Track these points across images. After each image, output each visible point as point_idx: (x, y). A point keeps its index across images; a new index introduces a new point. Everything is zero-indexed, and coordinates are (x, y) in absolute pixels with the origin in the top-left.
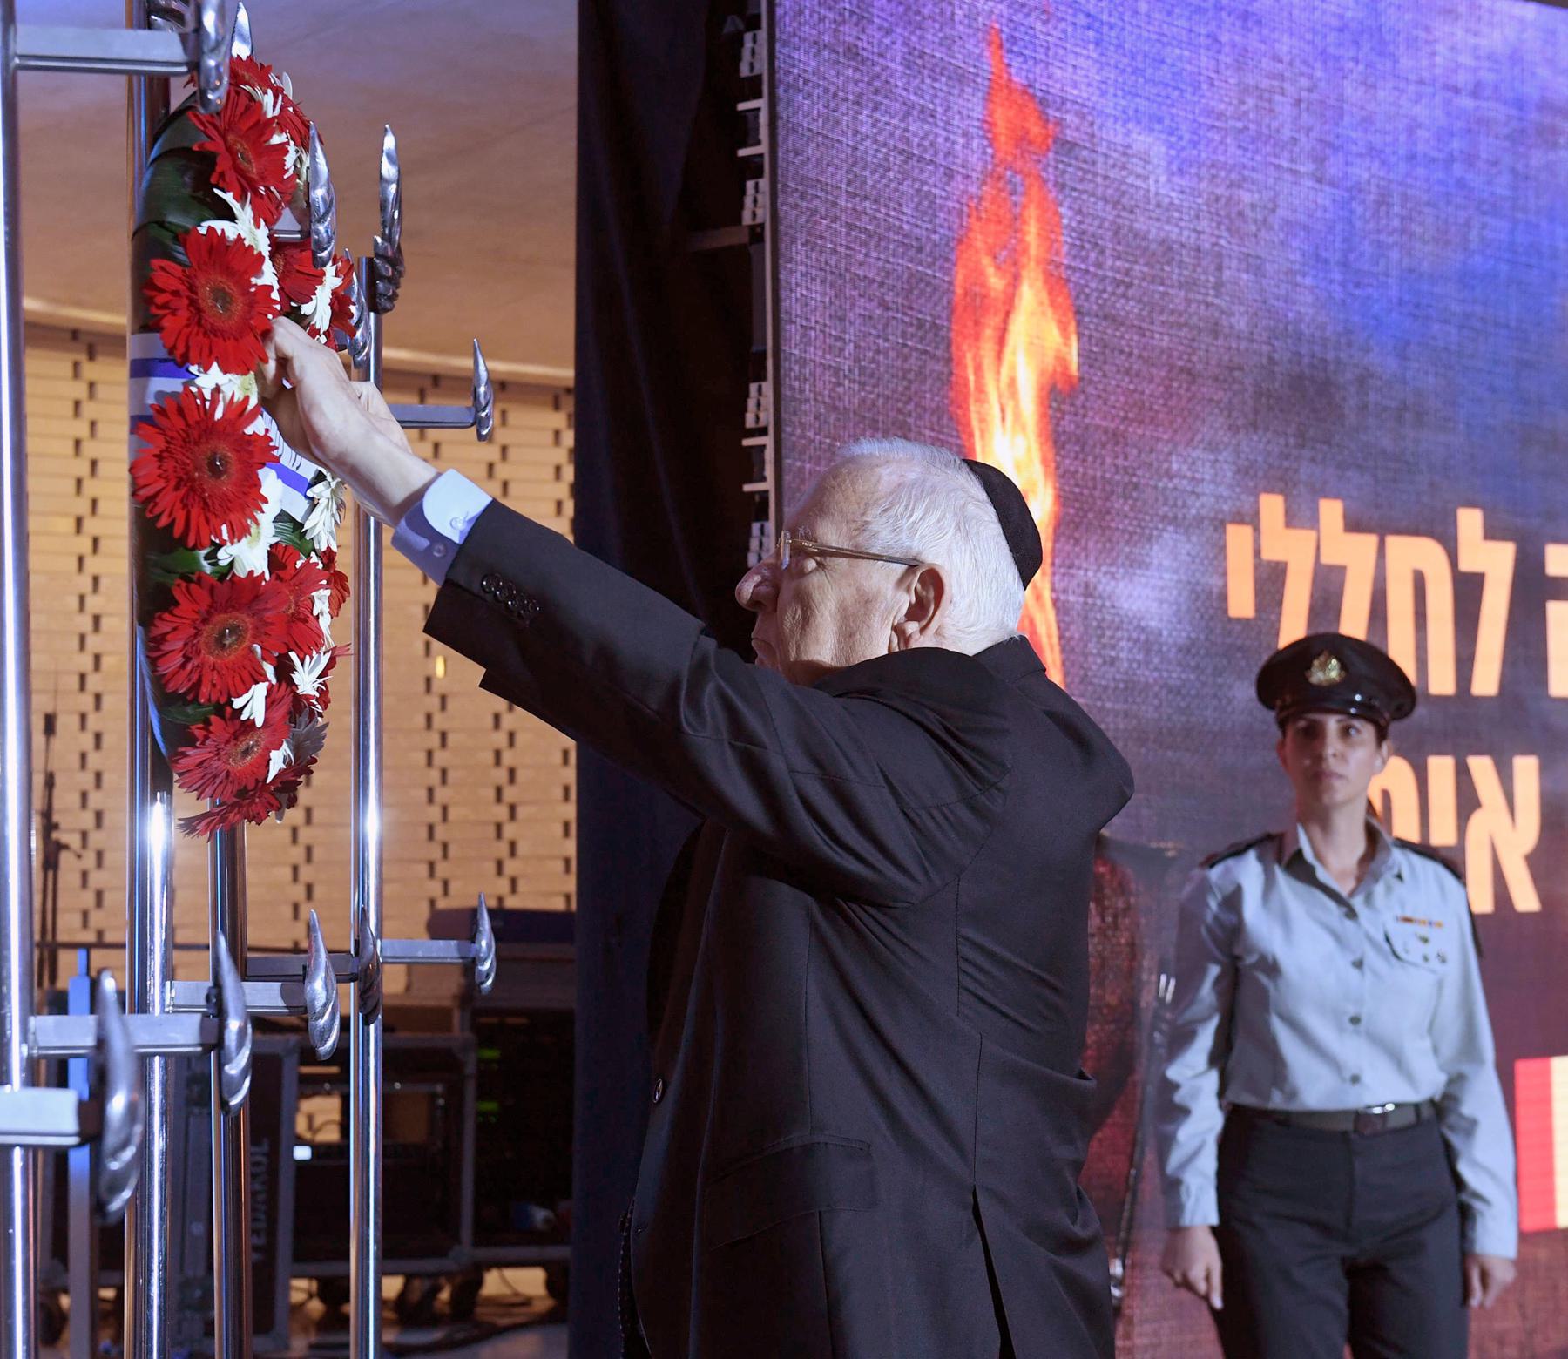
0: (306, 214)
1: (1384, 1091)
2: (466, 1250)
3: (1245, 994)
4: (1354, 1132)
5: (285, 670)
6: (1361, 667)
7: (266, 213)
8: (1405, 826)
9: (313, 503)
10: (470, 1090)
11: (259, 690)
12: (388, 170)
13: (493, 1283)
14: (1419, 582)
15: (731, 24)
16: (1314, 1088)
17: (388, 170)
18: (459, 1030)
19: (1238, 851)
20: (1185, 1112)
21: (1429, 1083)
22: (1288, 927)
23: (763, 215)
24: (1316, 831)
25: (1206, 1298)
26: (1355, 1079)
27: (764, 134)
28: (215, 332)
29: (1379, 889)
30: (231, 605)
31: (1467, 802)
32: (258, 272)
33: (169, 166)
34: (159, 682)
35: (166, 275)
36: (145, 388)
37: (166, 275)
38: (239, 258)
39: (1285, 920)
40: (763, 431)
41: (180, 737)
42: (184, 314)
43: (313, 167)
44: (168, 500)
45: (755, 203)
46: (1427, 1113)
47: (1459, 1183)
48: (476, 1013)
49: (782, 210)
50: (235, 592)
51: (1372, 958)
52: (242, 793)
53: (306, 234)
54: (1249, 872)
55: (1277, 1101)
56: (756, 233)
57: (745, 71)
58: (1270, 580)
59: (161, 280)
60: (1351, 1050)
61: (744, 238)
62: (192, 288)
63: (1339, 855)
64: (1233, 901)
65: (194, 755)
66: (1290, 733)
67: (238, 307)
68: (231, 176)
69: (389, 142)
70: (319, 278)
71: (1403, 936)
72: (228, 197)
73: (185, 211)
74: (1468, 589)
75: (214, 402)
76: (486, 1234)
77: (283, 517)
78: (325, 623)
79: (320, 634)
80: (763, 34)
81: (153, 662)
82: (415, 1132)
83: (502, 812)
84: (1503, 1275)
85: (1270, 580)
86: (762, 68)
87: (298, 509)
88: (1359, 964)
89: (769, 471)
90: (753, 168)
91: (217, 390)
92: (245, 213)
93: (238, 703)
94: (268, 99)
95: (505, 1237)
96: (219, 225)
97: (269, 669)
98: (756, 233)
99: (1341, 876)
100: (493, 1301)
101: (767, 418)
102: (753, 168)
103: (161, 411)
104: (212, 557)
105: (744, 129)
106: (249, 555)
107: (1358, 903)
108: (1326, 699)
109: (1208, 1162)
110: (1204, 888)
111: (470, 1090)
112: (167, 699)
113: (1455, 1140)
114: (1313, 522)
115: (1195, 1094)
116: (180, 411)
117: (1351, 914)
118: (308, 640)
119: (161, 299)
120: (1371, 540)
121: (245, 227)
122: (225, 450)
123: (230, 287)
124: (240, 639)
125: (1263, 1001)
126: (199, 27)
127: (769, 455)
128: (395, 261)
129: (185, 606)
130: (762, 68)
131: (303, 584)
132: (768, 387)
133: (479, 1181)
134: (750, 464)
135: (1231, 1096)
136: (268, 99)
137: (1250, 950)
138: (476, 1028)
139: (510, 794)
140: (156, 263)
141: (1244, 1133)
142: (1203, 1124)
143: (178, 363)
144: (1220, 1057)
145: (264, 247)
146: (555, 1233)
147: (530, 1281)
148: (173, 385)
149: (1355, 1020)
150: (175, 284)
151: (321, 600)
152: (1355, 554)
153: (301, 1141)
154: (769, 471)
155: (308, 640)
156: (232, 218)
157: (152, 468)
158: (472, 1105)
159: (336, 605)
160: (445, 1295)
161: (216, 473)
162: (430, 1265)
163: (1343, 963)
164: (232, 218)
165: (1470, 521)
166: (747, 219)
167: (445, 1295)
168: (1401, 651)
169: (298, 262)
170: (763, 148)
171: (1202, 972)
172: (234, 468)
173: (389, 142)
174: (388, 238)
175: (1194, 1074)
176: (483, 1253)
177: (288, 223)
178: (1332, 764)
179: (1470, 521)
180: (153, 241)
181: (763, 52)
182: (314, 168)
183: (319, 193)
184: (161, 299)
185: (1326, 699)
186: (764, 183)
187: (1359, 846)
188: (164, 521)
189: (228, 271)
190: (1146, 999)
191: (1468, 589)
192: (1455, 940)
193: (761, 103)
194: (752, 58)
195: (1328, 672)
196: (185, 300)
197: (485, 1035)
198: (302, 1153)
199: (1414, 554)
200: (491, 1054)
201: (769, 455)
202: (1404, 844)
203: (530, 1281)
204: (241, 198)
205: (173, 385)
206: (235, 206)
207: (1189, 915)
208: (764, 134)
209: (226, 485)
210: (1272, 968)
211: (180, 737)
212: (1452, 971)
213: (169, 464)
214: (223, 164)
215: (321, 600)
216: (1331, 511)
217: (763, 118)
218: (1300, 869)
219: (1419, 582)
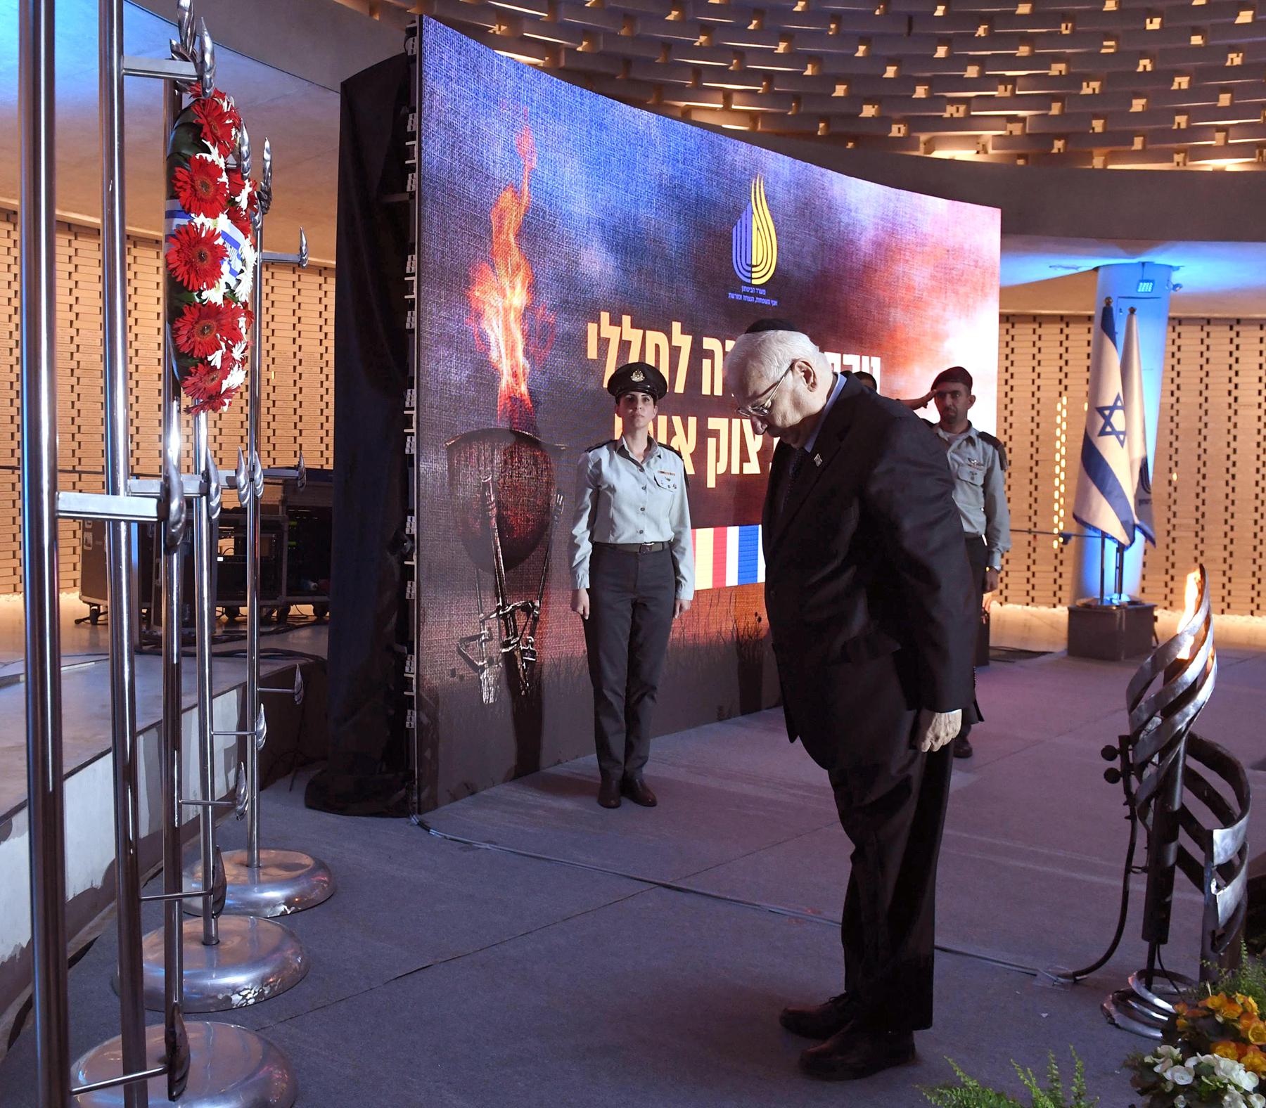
0: (240, 157)
1: (654, 535)
2: (283, 597)
3: (602, 497)
4: (638, 552)
5: (229, 349)
6: (651, 376)
7: (224, 153)
8: (662, 438)
9: (239, 281)
10: (286, 537)
11: (218, 354)
12: (267, 156)
13: (294, 610)
14: (657, 346)
15: (404, 110)
16: (625, 535)
17: (267, 156)
18: (281, 513)
19: (600, 447)
20: (578, 547)
21: (668, 535)
22: (618, 475)
23: (415, 188)
24: (630, 439)
25: (583, 617)
26: (641, 532)
27: (416, 155)
28: (202, 200)
29: (652, 461)
30: (208, 316)
31: (671, 433)
32: (221, 176)
33: (183, 130)
34: (177, 348)
35: (181, 174)
36: (171, 223)
37: (181, 174)
38: (212, 169)
39: (617, 471)
40: (413, 275)
41: (185, 372)
42: (189, 191)
43: (243, 138)
44: (181, 270)
45: (412, 183)
46: (666, 546)
47: (677, 571)
48: (289, 507)
49: (423, 186)
50: (211, 310)
51: (649, 486)
52: (210, 397)
53: (239, 165)
54: (604, 453)
55: (611, 539)
56: (412, 195)
57: (409, 129)
58: (603, 343)
59: (179, 176)
60: (642, 522)
61: (406, 197)
62: (192, 181)
63: (638, 448)
64: (598, 465)
65: (191, 380)
66: (622, 401)
67: (212, 190)
68: (209, 134)
69: (267, 145)
70: (243, 186)
71: (660, 478)
72: (208, 143)
73: (189, 149)
74: (675, 352)
75: (202, 230)
76: (291, 592)
77: (228, 285)
78: (243, 331)
79: (241, 335)
80: (417, 115)
81: (174, 340)
82: (266, 554)
83: (297, 433)
84: (686, 607)
85: (603, 343)
86: (416, 128)
87: (233, 284)
88: (644, 488)
89: (415, 291)
90: (412, 168)
91: (203, 225)
92: (215, 151)
93: (210, 358)
94: (225, 104)
95: (299, 594)
96: (204, 155)
97: (223, 344)
98: (412, 195)
99: (638, 456)
100: (293, 617)
101: (415, 269)
102: (412, 168)
103: (179, 232)
104: (199, 296)
105: (408, 153)
106: (214, 295)
107: (644, 465)
108: (637, 387)
109: (586, 565)
110: (587, 460)
111: (286, 537)
112: (180, 356)
113: (677, 556)
114: (619, 324)
115: (582, 540)
116: (187, 232)
117: (642, 470)
118: (236, 338)
119: (179, 184)
120: (641, 332)
121: (214, 156)
122: (206, 251)
123: (208, 181)
124: (211, 331)
125: (608, 503)
126: (203, 61)
127: (415, 284)
128: (269, 193)
129: (188, 317)
130: (416, 128)
131: (235, 314)
132: (415, 257)
133: (289, 572)
134: (408, 288)
135: (595, 539)
136: (225, 104)
137: (604, 483)
138: (287, 513)
139: (299, 426)
140: (177, 169)
141: (600, 550)
142: (586, 549)
143: (186, 212)
144: (590, 526)
145: (222, 166)
146: (317, 592)
147: (308, 610)
148: (184, 222)
149: (643, 509)
150: (185, 179)
151: (242, 321)
152: (634, 336)
153: (220, 555)
154: (415, 291)
155: (236, 338)
156: (210, 153)
157: (174, 257)
158: (287, 543)
159: (248, 324)
160: (275, 614)
161: (202, 259)
162: (270, 603)
163: (639, 488)
164: (210, 153)
165: (676, 326)
166: (408, 189)
167: (275, 614)
168: (664, 370)
169: (236, 173)
170: (416, 161)
171: (584, 493)
172: (210, 258)
173: (267, 145)
174: (266, 184)
175: (581, 530)
176: (291, 599)
177: (231, 159)
178: (639, 411)
179: (676, 326)
180: (175, 160)
181: (417, 122)
182: (242, 138)
183: (244, 149)
184: (179, 184)
185: (637, 387)
186: (416, 175)
187: (645, 445)
188: (179, 279)
189: (209, 175)
190: (553, 502)
191: (675, 352)
192: (679, 480)
193: (416, 143)
194: (412, 123)
195: (637, 378)
196: (188, 185)
197: (292, 516)
198: (220, 559)
199: (655, 337)
200: (293, 523)
201: (415, 284)
202: (661, 445)
203: (308, 610)
204: (214, 145)
205: (184, 222)
206: (211, 148)
207: (581, 469)
208: (416, 155)
209: (206, 265)
210: (612, 489)
211: (185, 372)
212: (678, 492)
213: (182, 255)
214: (206, 129)
215: (242, 321)
216: (626, 320)
217: (416, 149)
218: (623, 453)
219: (657, 346)
